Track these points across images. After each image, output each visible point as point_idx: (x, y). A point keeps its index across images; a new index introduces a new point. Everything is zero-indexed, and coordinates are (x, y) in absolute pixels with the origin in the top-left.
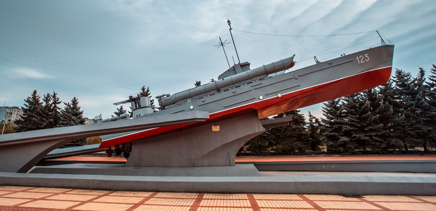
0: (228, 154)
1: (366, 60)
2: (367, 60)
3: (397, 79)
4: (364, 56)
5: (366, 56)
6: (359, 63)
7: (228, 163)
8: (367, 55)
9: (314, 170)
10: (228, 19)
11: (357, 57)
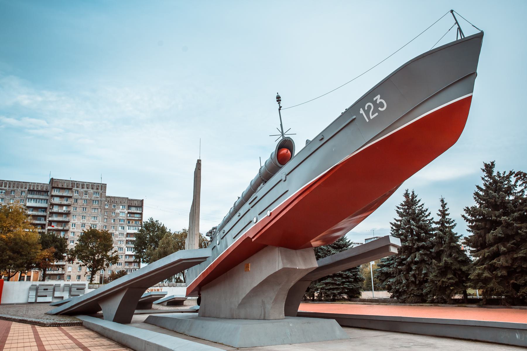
0: (263, 302)
1: (380, 109)
4: (375, 103)
5: (377, 99)
6: (367, 121)
7: (262, 317)
8: (378, 97)
9: (497, 342)
10: (278, 93)
11: (361, 109)
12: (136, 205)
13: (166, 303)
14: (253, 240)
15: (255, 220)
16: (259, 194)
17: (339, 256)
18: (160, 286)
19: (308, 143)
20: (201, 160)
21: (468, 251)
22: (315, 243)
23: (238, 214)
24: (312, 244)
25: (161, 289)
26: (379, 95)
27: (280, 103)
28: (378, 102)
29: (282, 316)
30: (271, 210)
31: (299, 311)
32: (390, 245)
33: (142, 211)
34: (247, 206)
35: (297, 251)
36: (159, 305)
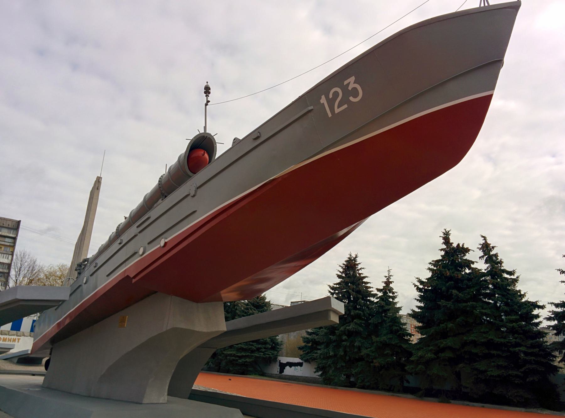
1: (351, 99)
2: (356, 96)
3: (552, 314)
4: (345, 89)
8: (352, 79)
10: (207, 82)
11: (323, 97)
12: (10, 227)
13: (16, 360)
14: (134, 281)
15: (141, 252)
16: (154, 214)
17: (257, 318)
18: (18, 335)
19: (235, 144)
20: (101, 178)
21: (411, 325)
22: (228, 295)
23: (119, 241)
24: (223, 295)
25: (19, 339)
26: (350, 90)
27: (209, 96)
28: (350, 88)
29: (163, 398)
30: (166, 239)
31: (194, 387)
32: (330, 310)
33: (17, 235)
34: (134, 230)
35: (199, 304)
36: (6, 361)
